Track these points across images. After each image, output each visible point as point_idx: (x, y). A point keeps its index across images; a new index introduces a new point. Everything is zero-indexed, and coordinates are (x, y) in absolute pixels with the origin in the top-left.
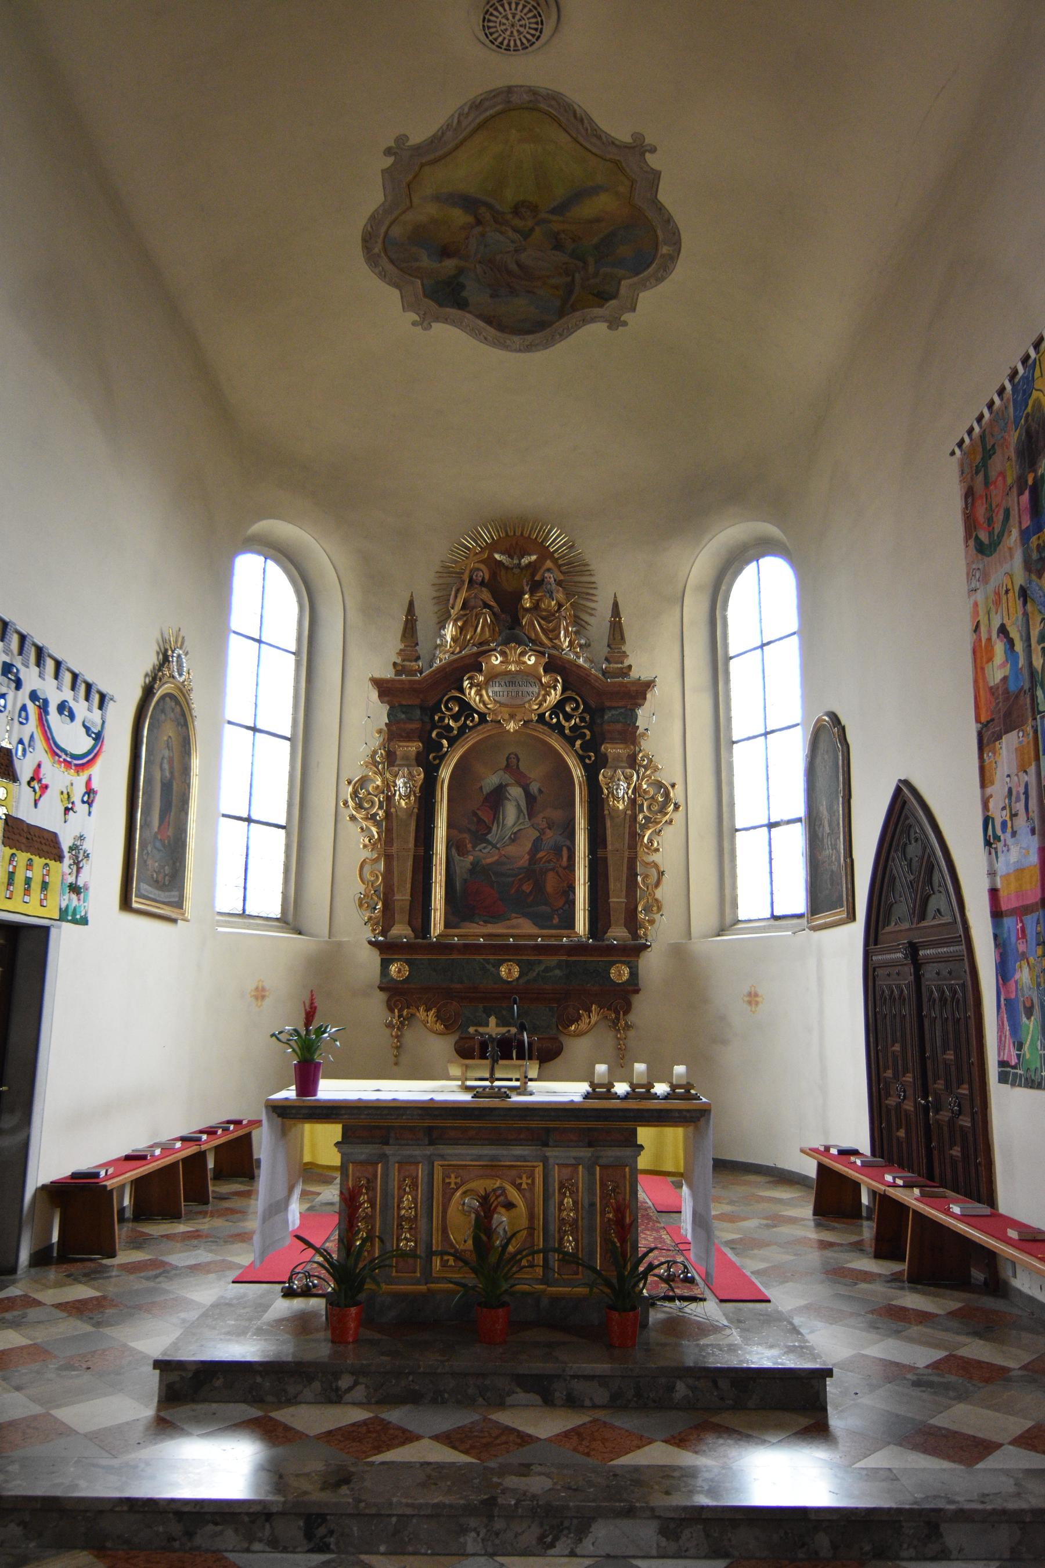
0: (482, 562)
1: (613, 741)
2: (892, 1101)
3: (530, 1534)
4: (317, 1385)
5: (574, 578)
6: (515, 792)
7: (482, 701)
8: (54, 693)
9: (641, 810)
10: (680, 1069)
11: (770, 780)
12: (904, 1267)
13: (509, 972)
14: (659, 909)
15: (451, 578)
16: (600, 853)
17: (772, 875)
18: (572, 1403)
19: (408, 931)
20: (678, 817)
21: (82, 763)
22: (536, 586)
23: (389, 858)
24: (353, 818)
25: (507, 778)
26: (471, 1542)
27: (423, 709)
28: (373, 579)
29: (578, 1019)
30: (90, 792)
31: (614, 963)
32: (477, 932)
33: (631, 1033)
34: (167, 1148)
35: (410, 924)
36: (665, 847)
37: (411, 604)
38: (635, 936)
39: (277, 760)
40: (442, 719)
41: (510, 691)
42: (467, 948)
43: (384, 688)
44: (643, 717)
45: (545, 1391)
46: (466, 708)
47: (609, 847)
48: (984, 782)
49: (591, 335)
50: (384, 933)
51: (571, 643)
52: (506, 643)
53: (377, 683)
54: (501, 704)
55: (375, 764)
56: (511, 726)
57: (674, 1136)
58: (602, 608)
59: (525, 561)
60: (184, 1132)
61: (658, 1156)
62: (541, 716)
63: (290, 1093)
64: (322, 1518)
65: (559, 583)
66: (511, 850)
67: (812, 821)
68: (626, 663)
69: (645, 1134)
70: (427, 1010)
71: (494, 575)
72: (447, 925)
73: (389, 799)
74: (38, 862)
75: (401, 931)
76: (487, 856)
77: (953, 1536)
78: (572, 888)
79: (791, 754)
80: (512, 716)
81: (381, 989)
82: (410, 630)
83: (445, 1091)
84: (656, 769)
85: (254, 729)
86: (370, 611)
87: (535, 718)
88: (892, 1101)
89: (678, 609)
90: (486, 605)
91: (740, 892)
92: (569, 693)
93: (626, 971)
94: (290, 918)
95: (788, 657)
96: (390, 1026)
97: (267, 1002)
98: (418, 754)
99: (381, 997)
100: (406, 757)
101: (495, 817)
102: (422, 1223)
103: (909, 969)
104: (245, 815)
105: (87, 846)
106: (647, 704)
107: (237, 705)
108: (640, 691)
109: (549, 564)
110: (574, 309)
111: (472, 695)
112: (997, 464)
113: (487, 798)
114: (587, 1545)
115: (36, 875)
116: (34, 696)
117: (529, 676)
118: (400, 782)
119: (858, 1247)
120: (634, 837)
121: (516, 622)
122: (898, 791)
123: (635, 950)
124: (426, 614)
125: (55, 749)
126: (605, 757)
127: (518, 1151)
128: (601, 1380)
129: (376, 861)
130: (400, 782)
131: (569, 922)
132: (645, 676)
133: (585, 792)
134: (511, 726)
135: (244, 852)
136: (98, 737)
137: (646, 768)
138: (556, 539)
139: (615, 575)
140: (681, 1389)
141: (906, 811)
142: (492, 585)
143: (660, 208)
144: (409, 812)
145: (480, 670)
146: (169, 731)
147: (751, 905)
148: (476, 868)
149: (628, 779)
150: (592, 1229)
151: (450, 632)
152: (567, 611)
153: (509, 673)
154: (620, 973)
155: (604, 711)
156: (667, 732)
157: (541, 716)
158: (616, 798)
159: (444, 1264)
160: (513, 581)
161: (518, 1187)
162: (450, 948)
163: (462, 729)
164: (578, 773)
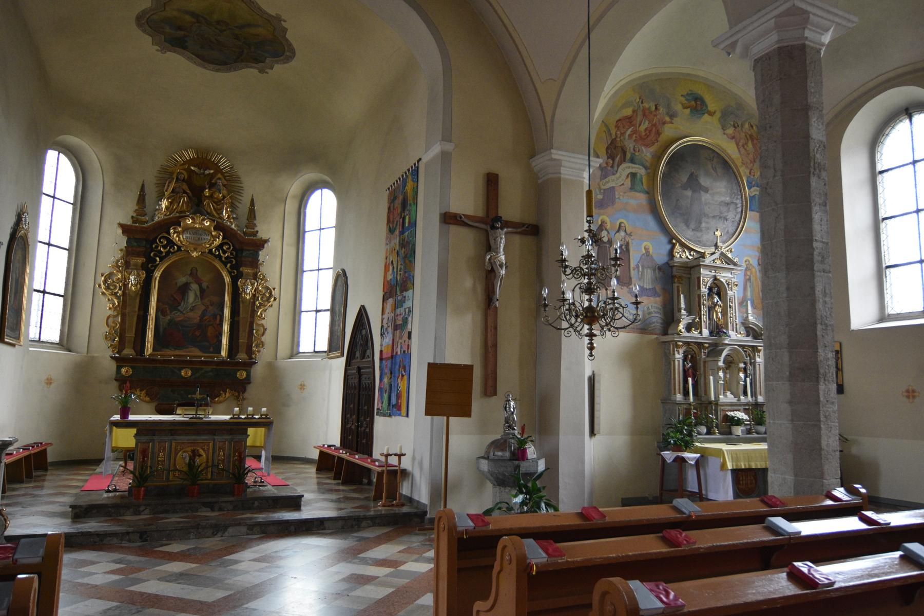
0: (185, 170)
1: (246, 266)
2: (349, 426)
4: (131, 510)
5: (232, 184)
6: (195, 286)
7: (179, 240)
10: (264, 409)
11: (317, 291)
13: (186, 373)
15: (165, 175)
16: (236, 318)
17: (314, 333)
18: (220, 509)
19: (133, 352)
20: (276, 304)
22: (212, 186)
23: (123, 316)
25: (191, 279)
26: (191, 536)
28: (121, 171)
29: (219, 395)
32: (171, 354)
33: (245, 402)
35: (134, 348)
37: (143, 186)
38: (250, 358)
40: (157, 247)
43: (125, 229)
44: (262, 255)
46: (171, 243)
48: (383, 314)
49: (250, 73)
52: (195, 213)
53: (122, 226)
54: (190, 243)
55: (118, 267)
56: (195, 254)
57: (261, 431)
58: (246, 200)
59: (207, 172)
61: (254, 441)
62: (210, 251)
63: (117, 417)
64: (146, 532)
65: (224, 185)
66: (191, 314)
67: (333, 311)
68: (256, 229)
69: (251, 431)
70: (141, 391)
71: (189, 176)
73: (125, 286)
75: (129, 352)
76: (178, 317)
77: (327, 524)
78: (221, 335)
79: (327, 280)
80: (195, 249)
81: (116, 380)
82: (141, 200)
84: (266, 281)
88: (349, 426)
90: (185, 192)
91: (301, 339)
93: (244, 374)
94: (65, 342)
95: (330, 236)
97: (53, 386)
98: (143, 264)
99: (115, 384)
100: (136, 265)
101: (183, 298)
102: (166, 462)
103: (357, 376)
104: (42, 289)
106: (264, 250)
108: (262, 244)
109: (219, 175)
110: (242, 61)
112: (397, 201)
114: (226, 534)
117: (206, 230)
118: (132, 278)
119: (329, 478)
120: (253, 312)
122: (360, 310)
126: (242, 273)
127: (204, 437)
128: (231, 502)
129: (115, 316)
130: (132, 278)
131: (219, 350)
132: (264, 237)
138: (224, 164)
139: (253, 185)
141: (362, 315)
142: (188, 182)
143: (287, 40)
145: (180, 226)
147: (305, 346)
149: (252, 284)
150: (229, 462)
151: (164, 204)
155: (243, 251)
156: (272, 263)
158: (246, 293)
159: (174, 475)
161: (203, 450)
163: (168, 253)
164: (227, 279)
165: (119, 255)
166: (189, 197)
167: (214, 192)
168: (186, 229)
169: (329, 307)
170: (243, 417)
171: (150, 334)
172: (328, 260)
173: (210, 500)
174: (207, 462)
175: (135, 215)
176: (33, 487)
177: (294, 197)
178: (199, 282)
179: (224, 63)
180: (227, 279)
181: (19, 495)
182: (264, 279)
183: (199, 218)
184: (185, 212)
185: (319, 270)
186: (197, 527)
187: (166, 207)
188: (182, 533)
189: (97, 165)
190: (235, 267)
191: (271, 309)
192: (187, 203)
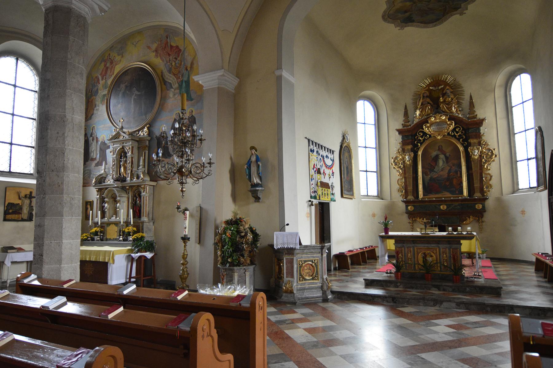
1: (472, 138)
3: (432, 303)
5: (456, 89)
6: (442, 156)
7: (429, 131)
8: (324, 153)
9: (483, 158)
11: (526, 146)
12: (547, 280)
13: (443, 207)
14: (491, 187)
15: (417, 96)
17: (527, 175)
18: (444, 290)
19: (413, 197)
21: (330, 167)
22: (444, 95)
23: (405, 178)
24: (394, 168)
25: (439, 153)
26: (421, 304)
27: (412, 135)
28: (394, 100)
29: (466, 220)
30: (333, 173)
31: (477, 204)
32: (433, 197)
33: (484, 224)
34: (357, 250)
36: (492, 168)
37: (406, 106)
38: (483, 195)
39: (372, 155)
41: (438, 127)
42: (430, 201)
43: (400, 132)
44: (483, 129)
45: (438, 288)
46: (425, 134)
47: (473, 170)
49: (455, 18)
50: (406, 198)
51: (456, 111)
52: (435, 114)
53: (398, 130)
55: (399, 152)
58: (467, 97)
59: (440, 88)
60: (361, 247)
62: (449, 133)
65: (452, 92)
66: (441, 173)
68: (475, 114)
69: (462, 241)
71: (430, 93)
72: (424, 195)
73: (404, 162)
74: (326, 189)
75: (411, 198)
76: (435, 175)
78: (462, 183)
80: (439, 135)
82: (406, 114)
83: (418, 234)
84: (488, 145)
85: (366, 147)
86: (394, 110)
87: (446, 134)
89: (493, 94)
90: (429, 103)
91: (519, 180)
92: (457, 125)
93: (481, 206)
94: (380, 195)
95: (530, 105)
96: (410, 223)
97: (376, 217)
99: (406, 216)
100: (408, 150)
101: (436, 164)
102: (413, 259)
105: (334, 185)
106: (483, 125)
107: (361, 142)
108: (481, 122)
109: (448, 87)
111: (426, 130)
113: (433, 159)
114: (442, 306)
115: (326, 192)
116: (322, 156)
117: (444, 122)
118: (407, 157)
120: (481, 167)
121: (438, 106)
123: (483, 200)
124: (410, 108)
125: (326, 166)
128: (450, 287)
130: (407, 157)
131: (462, 192)
132: (482, 117)
133: (464, 154)
134: (439, 137)
135: (367, 183)
136: (333, 161)
137: (484, 145)
138: (450, 79)
139: (470, 87)
140: (468, 289)
142: (430, 97)
144: (410, 165)
145: (428, 123)
146: (346, 154)
148: (431, 179)
149: (478, 149)
152: (455, 100)
153: (436, 122)
154: (479, 206)
156: (491, 133)
157: (449, 133)
160: (437, 94)
161: (433, 253)
162: (426, 201)
163: (424, 140)
164: (461, 149)
165: (399, 146)
166: (431, 105)
167: (446, 98)
168: (432, 124)
169: (534, 156)
170: (464, 233)
171: (465, 184)
172: (531, 123)
173: (439, 284)
174: (437, 260)
175: (403, 123)
176: (363, 268)
177: (500, 86)
178: (444, 153)
179: (437, 20)
180: (461, 149)
181: (354, 271)
182: (486, 144)
183: (438, 116)
184: (429, 114)
185: (525, 131)
186: (424, 299)
187: (420, 115)
188: (415, 301)
189: (382, 102)
190: (466, 140)
191: (494, 162)
192: (431, 109)
